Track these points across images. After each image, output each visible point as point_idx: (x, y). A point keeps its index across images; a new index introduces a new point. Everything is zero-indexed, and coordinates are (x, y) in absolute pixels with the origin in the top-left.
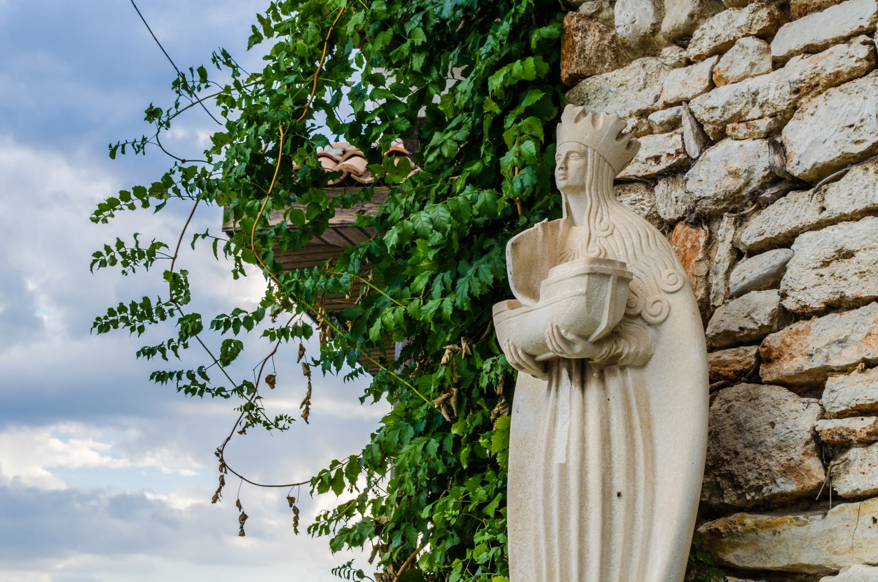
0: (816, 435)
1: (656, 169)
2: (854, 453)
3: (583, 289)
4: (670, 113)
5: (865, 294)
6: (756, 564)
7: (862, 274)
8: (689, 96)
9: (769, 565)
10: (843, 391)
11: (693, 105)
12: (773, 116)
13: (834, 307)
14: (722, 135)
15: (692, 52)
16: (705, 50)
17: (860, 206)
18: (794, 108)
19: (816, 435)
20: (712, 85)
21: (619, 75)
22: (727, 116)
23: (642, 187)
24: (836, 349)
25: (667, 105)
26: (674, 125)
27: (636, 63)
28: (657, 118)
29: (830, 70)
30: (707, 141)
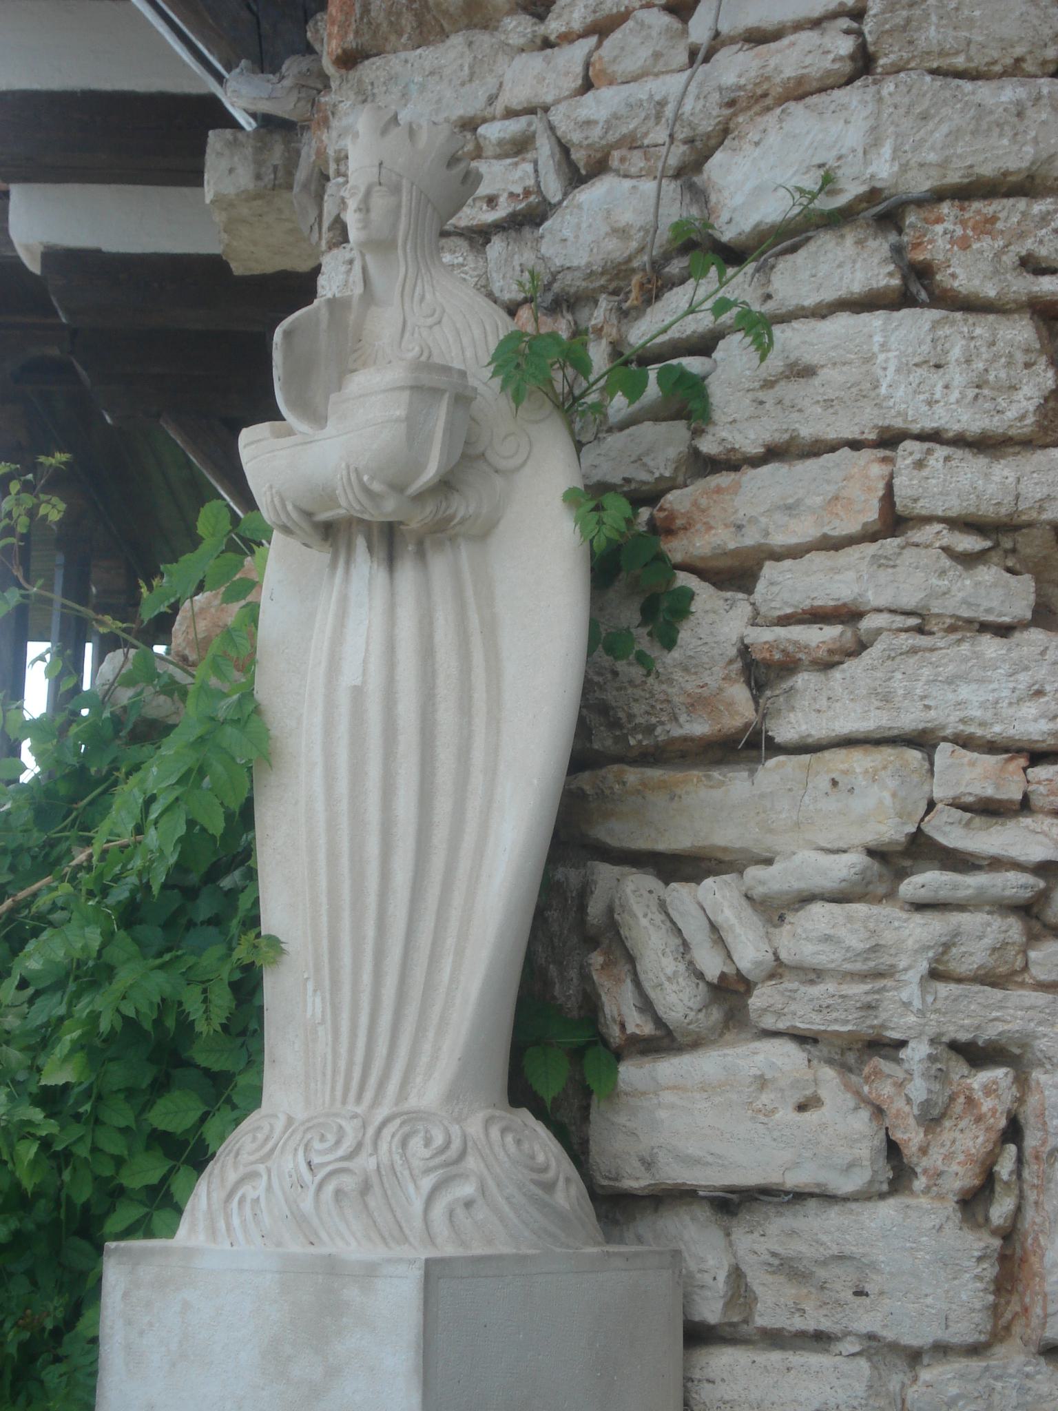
0: (744, 650)
1: (490, 217)
2: (802, 680)
3: (400, 412)
4: (514, 127)
5: (832, 435)
6: (641, 844)
7: (828, 404)
8: (549, 99)
9: (661, 846)
10: (783, 586)
11: (556, 116)
12: (690, 141)
13: (773, 454)
14: (600, 167)
15: (554, 26)
16: (577, 26)
17: (829, 295)
18: (724, 132)
19: (744, 650)
20: (587, 85)
21: (428, 56)
22: (612, 137)
23: (463, 244)
24: (780, 518)
25: (510, 114)
26: (520, 147)
27: (457, 40)
28: (492, 132)
29: (789, 72)
30: (576, 177)
